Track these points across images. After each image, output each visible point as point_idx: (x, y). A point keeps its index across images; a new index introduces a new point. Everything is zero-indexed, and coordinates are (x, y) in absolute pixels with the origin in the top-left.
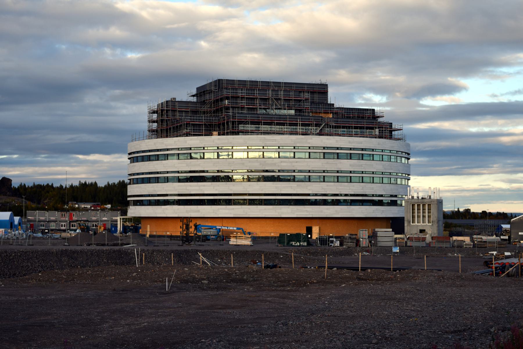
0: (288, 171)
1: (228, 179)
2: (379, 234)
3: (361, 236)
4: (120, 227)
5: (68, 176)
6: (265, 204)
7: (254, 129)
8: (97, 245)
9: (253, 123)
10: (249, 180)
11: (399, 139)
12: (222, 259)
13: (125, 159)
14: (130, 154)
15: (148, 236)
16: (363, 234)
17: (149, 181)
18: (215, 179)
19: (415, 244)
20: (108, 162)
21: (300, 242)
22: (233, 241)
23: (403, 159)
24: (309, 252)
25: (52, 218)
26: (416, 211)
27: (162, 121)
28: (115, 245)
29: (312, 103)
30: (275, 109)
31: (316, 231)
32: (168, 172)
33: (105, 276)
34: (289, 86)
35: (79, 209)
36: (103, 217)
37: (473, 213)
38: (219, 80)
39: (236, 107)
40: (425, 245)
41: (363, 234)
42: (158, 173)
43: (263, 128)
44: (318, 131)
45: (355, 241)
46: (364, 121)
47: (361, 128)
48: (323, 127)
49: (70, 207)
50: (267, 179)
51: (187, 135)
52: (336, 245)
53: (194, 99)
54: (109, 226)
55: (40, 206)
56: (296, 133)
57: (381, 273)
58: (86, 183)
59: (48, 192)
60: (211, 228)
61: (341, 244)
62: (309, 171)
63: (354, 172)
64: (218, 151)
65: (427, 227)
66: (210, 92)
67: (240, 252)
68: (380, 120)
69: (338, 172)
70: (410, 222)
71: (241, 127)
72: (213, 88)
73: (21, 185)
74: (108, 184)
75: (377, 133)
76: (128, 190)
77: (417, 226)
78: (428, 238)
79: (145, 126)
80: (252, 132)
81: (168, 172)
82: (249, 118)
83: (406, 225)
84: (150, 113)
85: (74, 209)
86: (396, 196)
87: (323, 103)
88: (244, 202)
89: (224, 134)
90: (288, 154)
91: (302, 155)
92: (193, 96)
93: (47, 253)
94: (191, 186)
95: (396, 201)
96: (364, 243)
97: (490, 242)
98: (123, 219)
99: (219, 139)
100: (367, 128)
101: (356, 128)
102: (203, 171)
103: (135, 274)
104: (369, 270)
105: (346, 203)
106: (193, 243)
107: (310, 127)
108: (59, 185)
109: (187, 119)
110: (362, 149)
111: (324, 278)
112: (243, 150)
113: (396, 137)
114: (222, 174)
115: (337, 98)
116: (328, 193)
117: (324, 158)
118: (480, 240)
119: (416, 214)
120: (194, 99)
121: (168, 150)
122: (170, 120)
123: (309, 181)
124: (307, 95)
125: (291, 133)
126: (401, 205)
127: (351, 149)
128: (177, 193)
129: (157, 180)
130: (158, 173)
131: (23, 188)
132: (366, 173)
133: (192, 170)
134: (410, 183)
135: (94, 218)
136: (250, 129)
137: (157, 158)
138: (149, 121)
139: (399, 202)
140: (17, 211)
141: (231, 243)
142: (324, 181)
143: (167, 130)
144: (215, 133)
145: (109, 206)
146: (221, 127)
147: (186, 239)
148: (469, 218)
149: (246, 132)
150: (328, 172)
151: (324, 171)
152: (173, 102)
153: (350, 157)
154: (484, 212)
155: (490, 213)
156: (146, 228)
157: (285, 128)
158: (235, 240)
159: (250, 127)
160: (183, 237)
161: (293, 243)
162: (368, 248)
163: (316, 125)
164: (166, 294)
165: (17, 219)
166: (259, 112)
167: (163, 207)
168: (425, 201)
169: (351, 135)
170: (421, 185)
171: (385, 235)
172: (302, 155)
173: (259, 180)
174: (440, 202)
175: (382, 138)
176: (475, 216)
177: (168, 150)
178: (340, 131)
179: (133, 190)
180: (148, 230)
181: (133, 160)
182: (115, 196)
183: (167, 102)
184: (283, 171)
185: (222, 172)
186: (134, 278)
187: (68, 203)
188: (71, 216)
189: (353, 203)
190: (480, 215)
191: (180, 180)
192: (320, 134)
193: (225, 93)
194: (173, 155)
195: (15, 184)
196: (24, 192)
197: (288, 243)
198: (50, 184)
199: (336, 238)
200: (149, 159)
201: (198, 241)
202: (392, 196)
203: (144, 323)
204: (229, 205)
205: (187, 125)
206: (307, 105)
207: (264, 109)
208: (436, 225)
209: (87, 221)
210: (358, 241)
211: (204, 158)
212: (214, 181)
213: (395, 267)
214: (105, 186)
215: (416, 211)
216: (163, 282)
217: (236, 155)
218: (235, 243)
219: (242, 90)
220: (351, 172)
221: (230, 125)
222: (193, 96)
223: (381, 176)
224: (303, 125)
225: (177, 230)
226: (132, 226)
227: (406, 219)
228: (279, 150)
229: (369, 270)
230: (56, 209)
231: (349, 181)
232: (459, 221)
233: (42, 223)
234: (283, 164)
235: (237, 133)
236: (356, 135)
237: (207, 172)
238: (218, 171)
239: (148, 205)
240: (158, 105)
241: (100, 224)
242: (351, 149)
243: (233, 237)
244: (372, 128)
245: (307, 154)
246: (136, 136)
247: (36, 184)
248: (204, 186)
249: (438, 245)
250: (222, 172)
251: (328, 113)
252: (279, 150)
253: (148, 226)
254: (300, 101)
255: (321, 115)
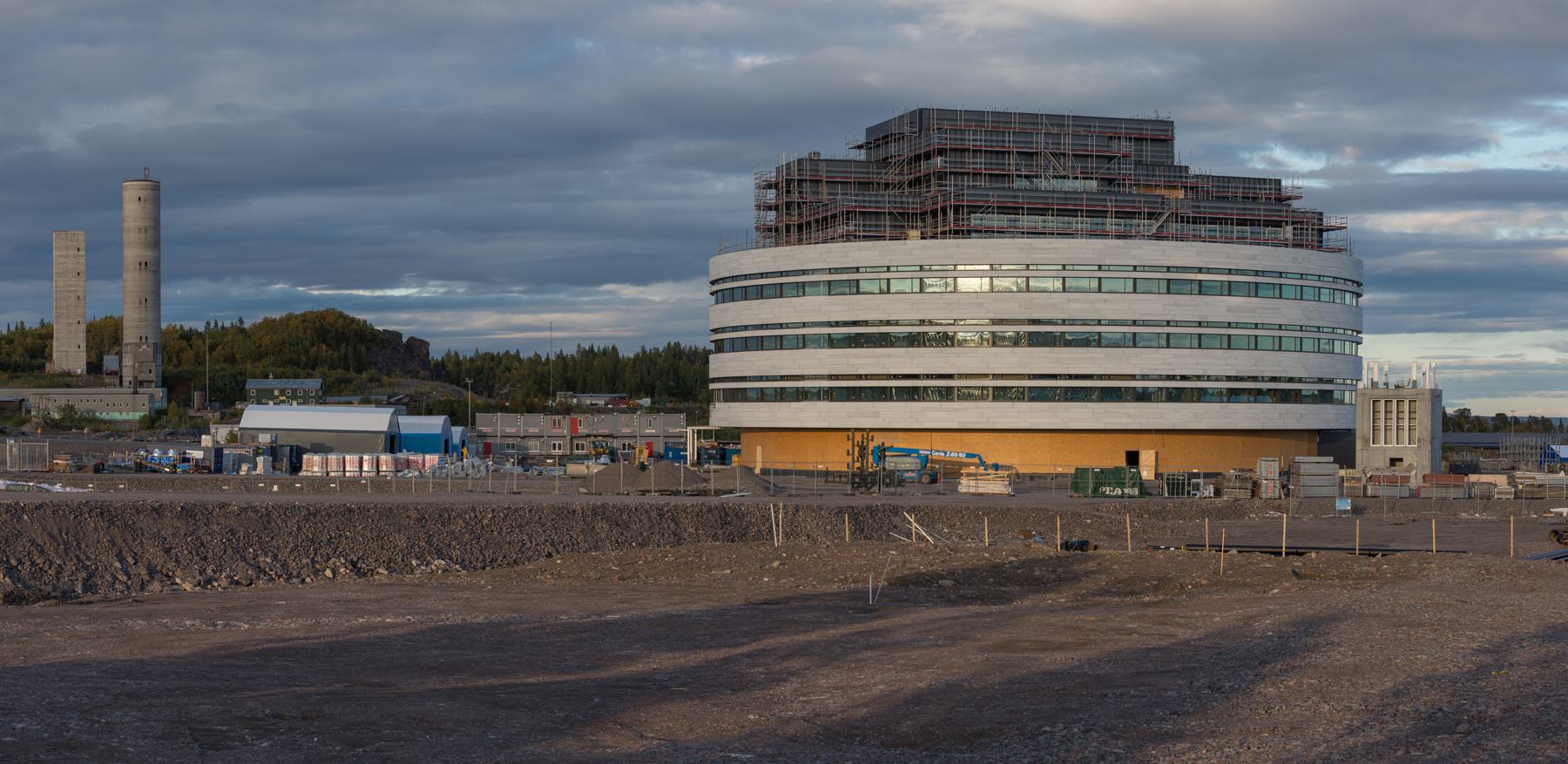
0: (1085, 322)
1: (946, 340)
2: (1304, 469)
3: (1264, 474)
4: (690, 453)
5: (556, 334)
6: (1032, 399)
7: (1005, 224)
8: (662, 492)
9: (1003, 210)
10: (996, 340)
11: (1340, 250)
12: (952, 526)
13: (696, 293)
14: (713, 283)
15: (757, 471)
16: (1268, 470)
17: (760, 344)
18: (914, 340)
19: (1384, 491)
20: (661, 303)
21: (1122, 486)
22: (966, 486)
23: (1348, 296)
24: (1148, 512)
25: (533, 430)
26: (1382, 415)
27: (789, 205)
28: (699, 493)
29: (1138, 163)
30: (1055, 177)
31: (1147, 458)
32: (804, 325)
33: (709, 568)
34: (1083, 124)
35: (579, 409)
36: (645, 427)
37: (1478, 418)
38: (921, 110)
39: (962, 174)
40: (1406, 494)
41: (1268, 470)
42: (781, 326)
43: (1026, 221)
44: (1154, 230)
45: (1250, 486)
46: (1257, 208)
47: (1253, 223)
48: (1166, 221)
49: (561, 404)
50: (1036, 340)
51: (849, 237)
52: (1206, 494)
53: (862, 155)
54: (659, 448)
55: (493, 401)
56: (1105, 235)
57: (1343, 560)
58: (592, 349)
59: (508, 370)
60: (907, 453)
61: (1218, 493)
62: (1135, 323)
63: (1238, 325)
64: (922, 274)
65: (1404, 449)
66: (901, 137)
67: (982, 507)
68: (1295, 204)
69: (1200, 324)
70: (1367, 441)
71: (975, 220)
72: (906, 129)
73: (448, 354)
74: (644, 351)
75: (1289, 235)
76: (712, 366)
77: (1385, 450)
78: (1415, 482)
79: (750, 218)
80: (1001, 232)
81: (804, 325)
82: (994, 198)
83: (1358, 447)
84: (759, 187)
85: (579, 409)
86: (1330, 381)
87: (1162, 164)
88: (981, 395)
89: (934, 237)
90: (1084, 283)
91: (906, 286)
92: (860, 147)
93: (564, 513)
94: (858, 356)
95: (1331, 392)
96: (1270, 489)
97: (1552, 487)
98: (699, 432)
99: (924, 247)
100: (1267, 224)
101: (1242, 223)
102: (888, 323)
103: (776, 564)
104: (1313, 555)
105: (1022, 395)
106: (876, 489)
107: (1135, 221)
108: (531, 355)
109: (846, 200)
110: (1257, 273)
111: (1216, 572)
112: (981, 274)
113: (1332, 244)
114: (932, 330)
115: (1194, 152)
116: (805, 373)
117: (1168, 292)
118: (1530, 482)
119: (1382, 423)
120: (862, 155)
121: (804, 272)
122: (806, 204)
123: (1134, 346)
124: (1125, 147)
125: (1092, 234)
126: (1342, 402)
127: (1230, 272)
128: (826, 373)
129: (780, 343)
130: (781, 326)
131: (453, 360)
132: (1263, 326)
133: (1035, 316)
134: (1362, 351)
135: (626, 431)
136: (995, 224)
137: (780, 291)
138: (758, 207)
139: (1337, 395)
140: (457, 415)
141: (962, 489)
142: (1168, 346)
143: (800, 227)
144: (914, 233)
145: (646, 402)
146: (940, 218)
147: (862, 480)
148: (1469, 430)
149: (989, 232)
150: (1177, 324)
151: (1168, 323)
152: (815, 160)
153: (1230, 289)
154: (1501, 417)
155: (1516, 420)
156: (754, 453)
157: (1079, 223)
158: (972, 483)
159: (996, 220)
160: (854, 475)
161: (1108, 490)
162: (1278, 502)
163: (1151, 216)
164: (871, 611)
165: (457, 431)
166: (1018, 184)
167: (794, 405)
168: (1404, 392)
169: (1229, 241)
170: (1390, 354)
171: (1316, 469)
172: (906, 286)
173: (1016, 342)
174: (1436, 395)
175: (1301, 246)
176: (1480, 424)
177: (804, 272)
178: (1203, 229)
179: (722, 365)
180: (758, 457)
181: (723, 296)
182: (676, 379)
183: (800, 161)
184: (1073, 322)
185: (931, 323)
186: (778, 574)
187: (554, 395)
188: (574, 425)
189: (1233, 395)
190: (1491, 423)
191: (832, 342)
192: (1158, 237)
193: (936, 141)
194: (816, 284)
195: (437, 352)
196: (450, 371)
197: (1095, 490)
198: (513, 352)
199: (1207, 475)
200: (760, 293)
201: (888, 485)
202: (1320, 380)
203: (875, 685)
204: (948, 400)
205: (849, 215)
206: (1127, 169)
207: (1027, 177)
208: (1427, 448)
209: (611, 436)
210: (1256, 485)
211: (889, 292)
212: (912, 345)
213: (1442, 547)
214: (637, 356)
215: (1382, 415)
216: (866, 580)
217: (966, 284)
218: (972, 490)
219: (975, 132)
220: (1229, 325)
221: (951, 215)
222: (860, 147)
223: (1299, 334)
224: (1119, 215)
225: (837, 458)
226: (713, 447)
227: (1358, 434)
228: (1064, 274)
229: (1313, 555)
230: (531, 410)
231: (1225, 345)
232: (1466, 439)
233: (510, 441)
234: (1073, 306)
235: (967, 233)
236: (1242, 240)
237: (897, 323)
238: (922, 322)
239: (757, 401)
240: (778, 170)
241: (640, 444)
242: (1230, 272)
243: (969, 475)
244: (1278, 224)
245: (1130, 284)
246: (729, 241)
247: (483, 351)
248: (889, 356)
249: (1435, 493)
250: (931, 323)
251: (1175, 187)
252: (1064, 274)
253: (759, 449)
254: (1110, 158)
255: (1158, 192)
